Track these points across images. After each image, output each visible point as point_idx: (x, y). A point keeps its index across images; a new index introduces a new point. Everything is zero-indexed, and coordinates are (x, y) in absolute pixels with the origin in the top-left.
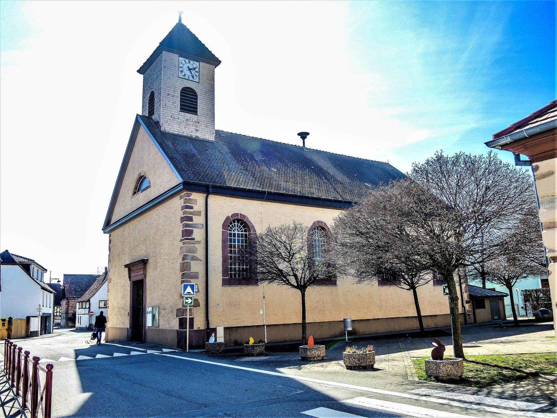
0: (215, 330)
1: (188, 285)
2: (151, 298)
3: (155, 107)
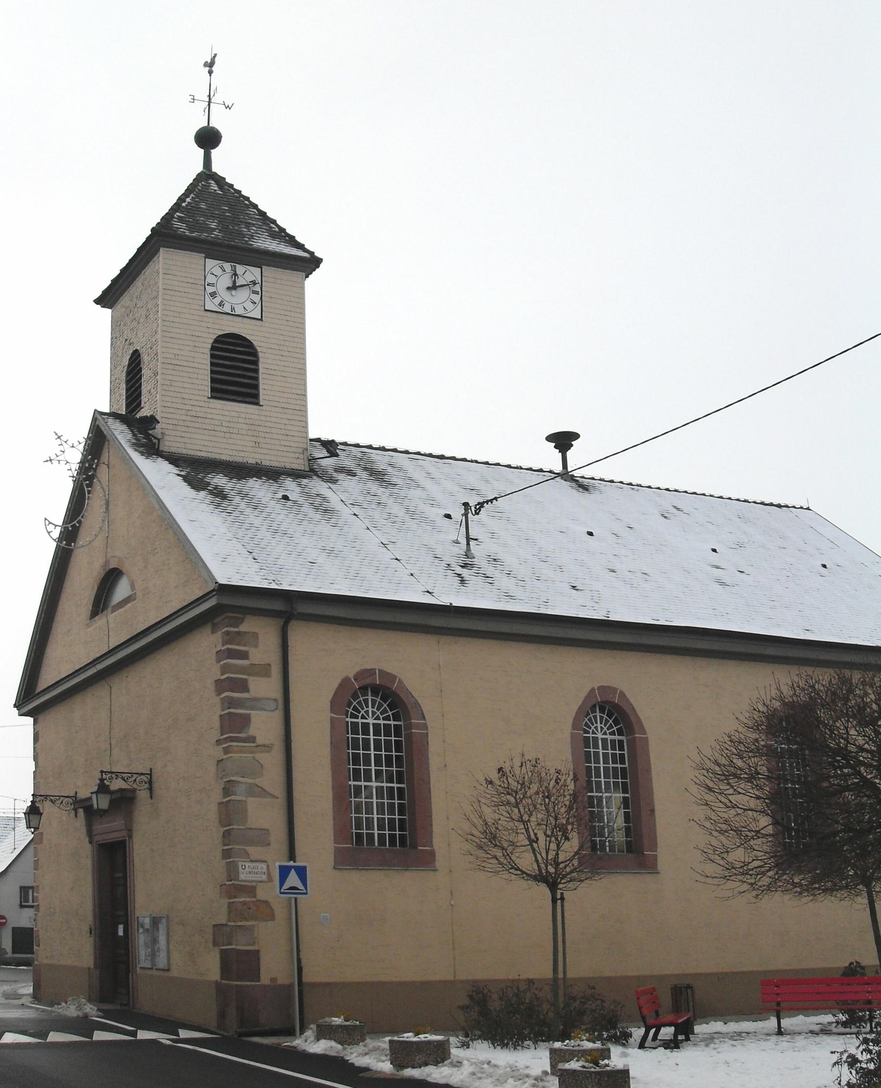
2: (147, 895)
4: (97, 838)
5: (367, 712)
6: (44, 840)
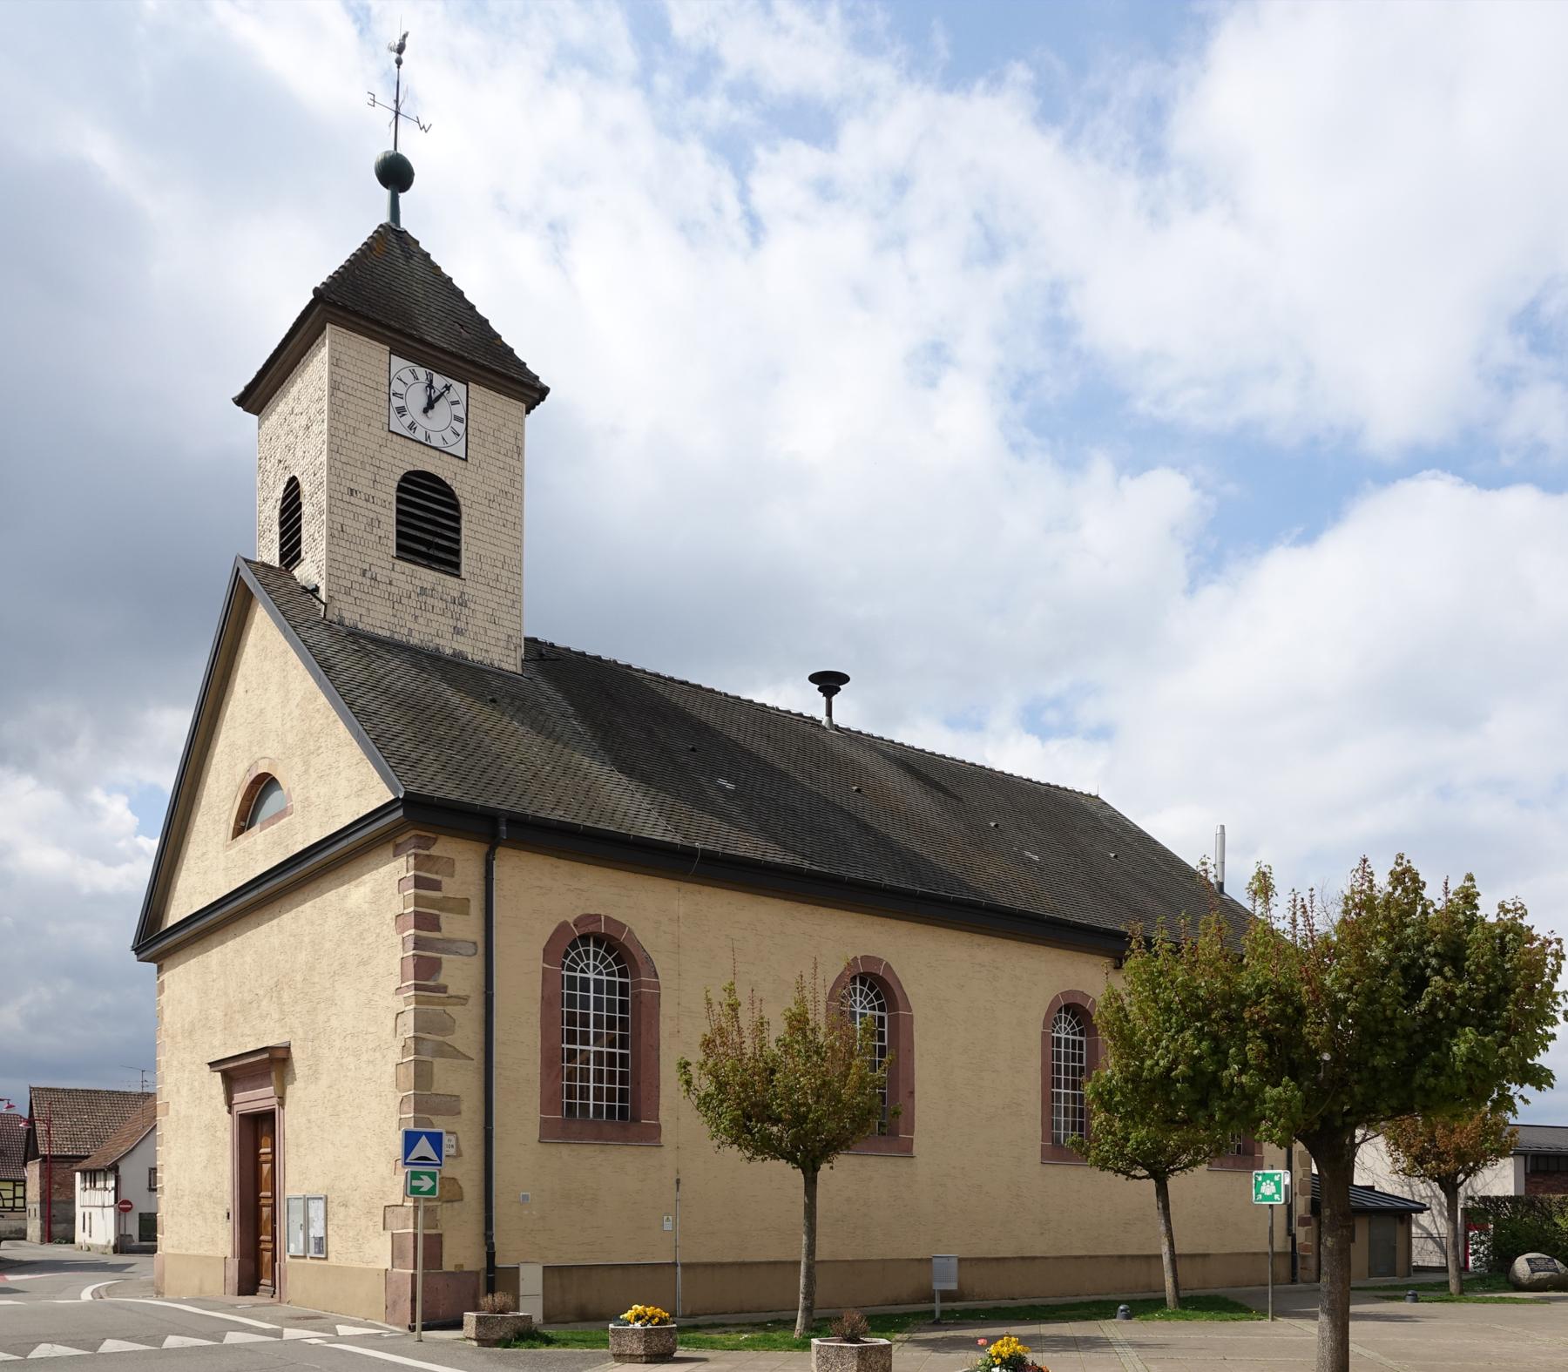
0: (514, 1273)
1: (421, 1134)
3: (304, 534)
4: (236, 1108)
5: (587, 965)
6: (171, 1112)
